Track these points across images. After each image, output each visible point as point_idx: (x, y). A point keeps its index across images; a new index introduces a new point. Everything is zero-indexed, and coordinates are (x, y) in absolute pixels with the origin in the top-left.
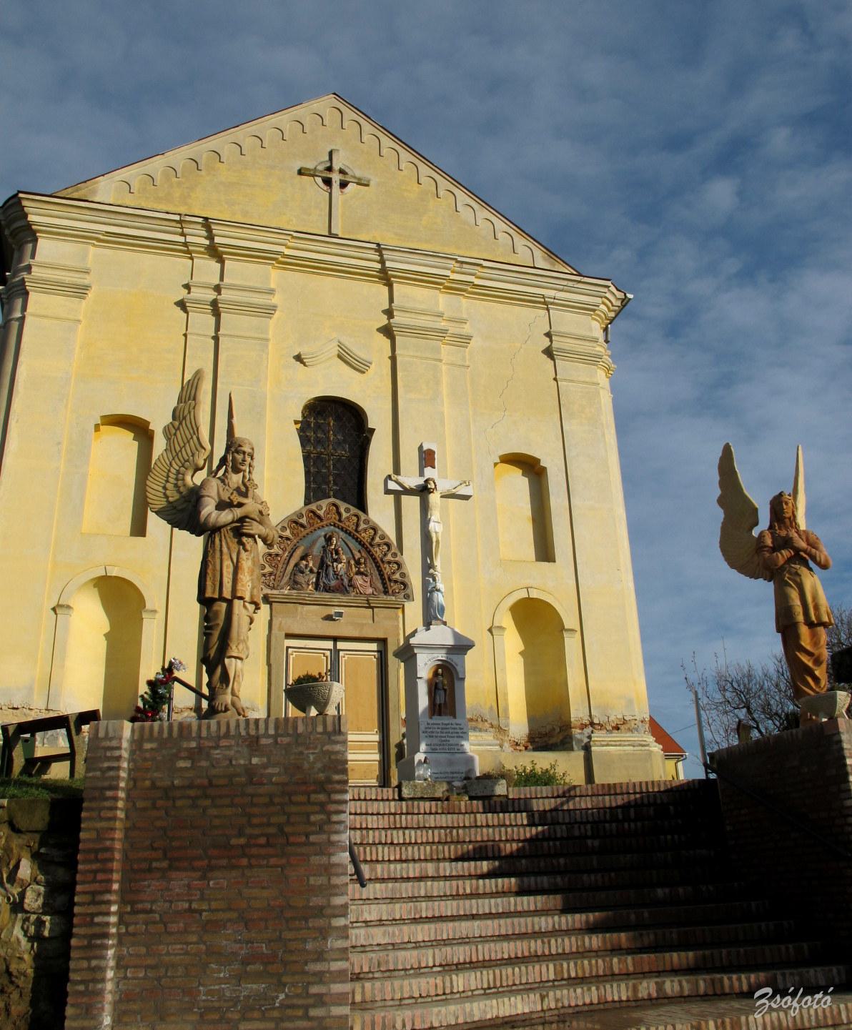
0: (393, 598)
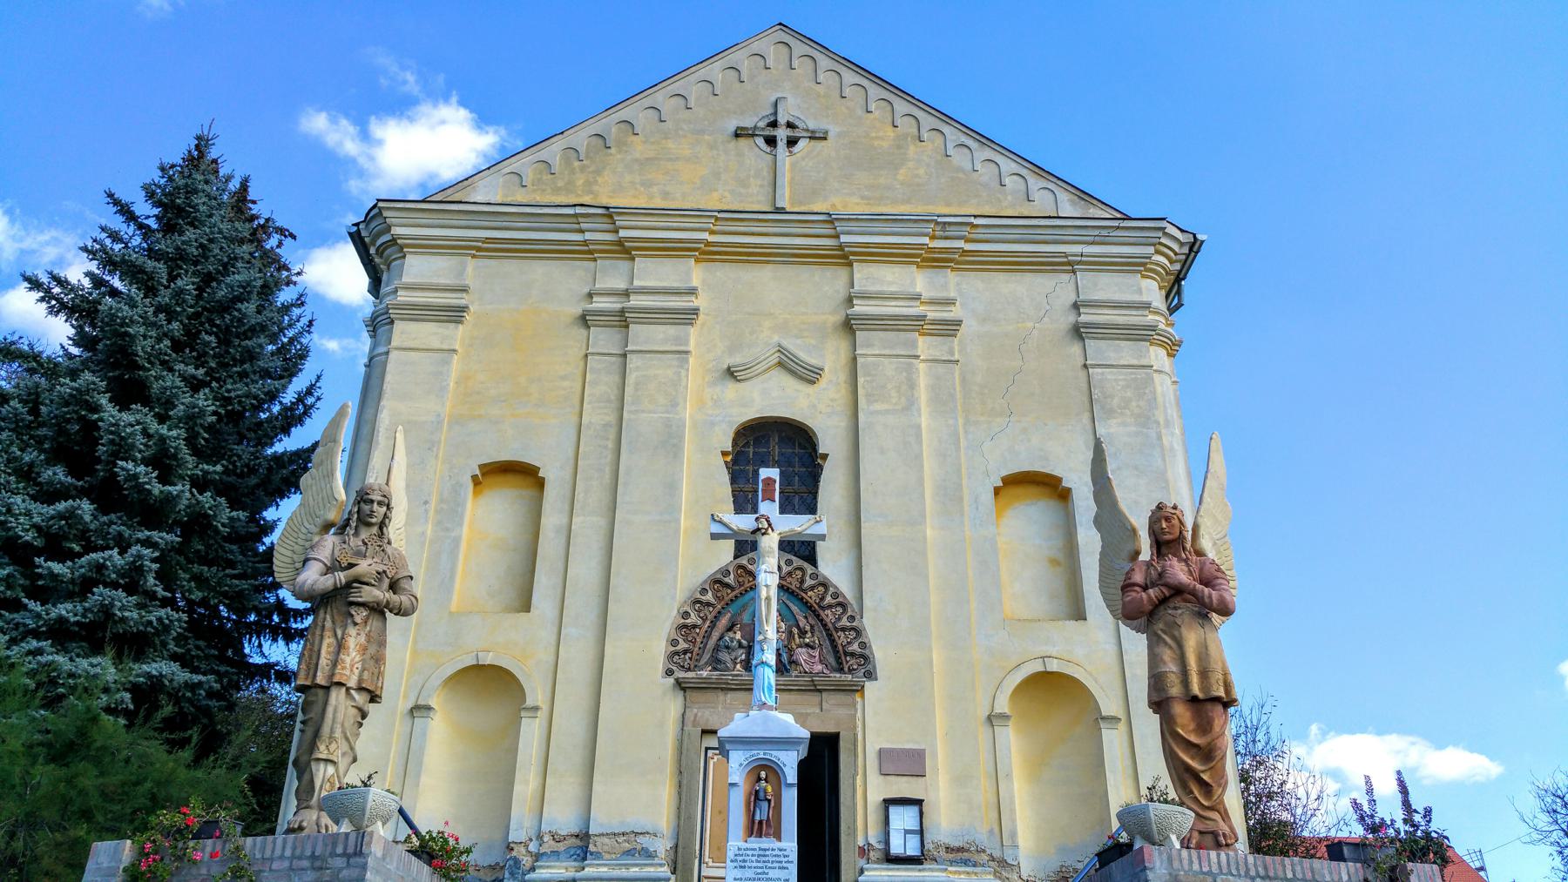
0: (849, 677)
